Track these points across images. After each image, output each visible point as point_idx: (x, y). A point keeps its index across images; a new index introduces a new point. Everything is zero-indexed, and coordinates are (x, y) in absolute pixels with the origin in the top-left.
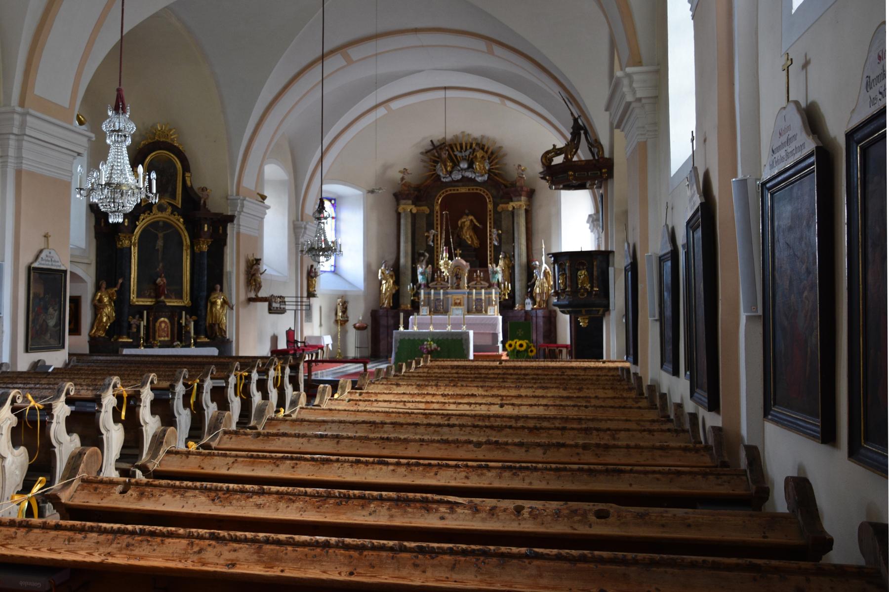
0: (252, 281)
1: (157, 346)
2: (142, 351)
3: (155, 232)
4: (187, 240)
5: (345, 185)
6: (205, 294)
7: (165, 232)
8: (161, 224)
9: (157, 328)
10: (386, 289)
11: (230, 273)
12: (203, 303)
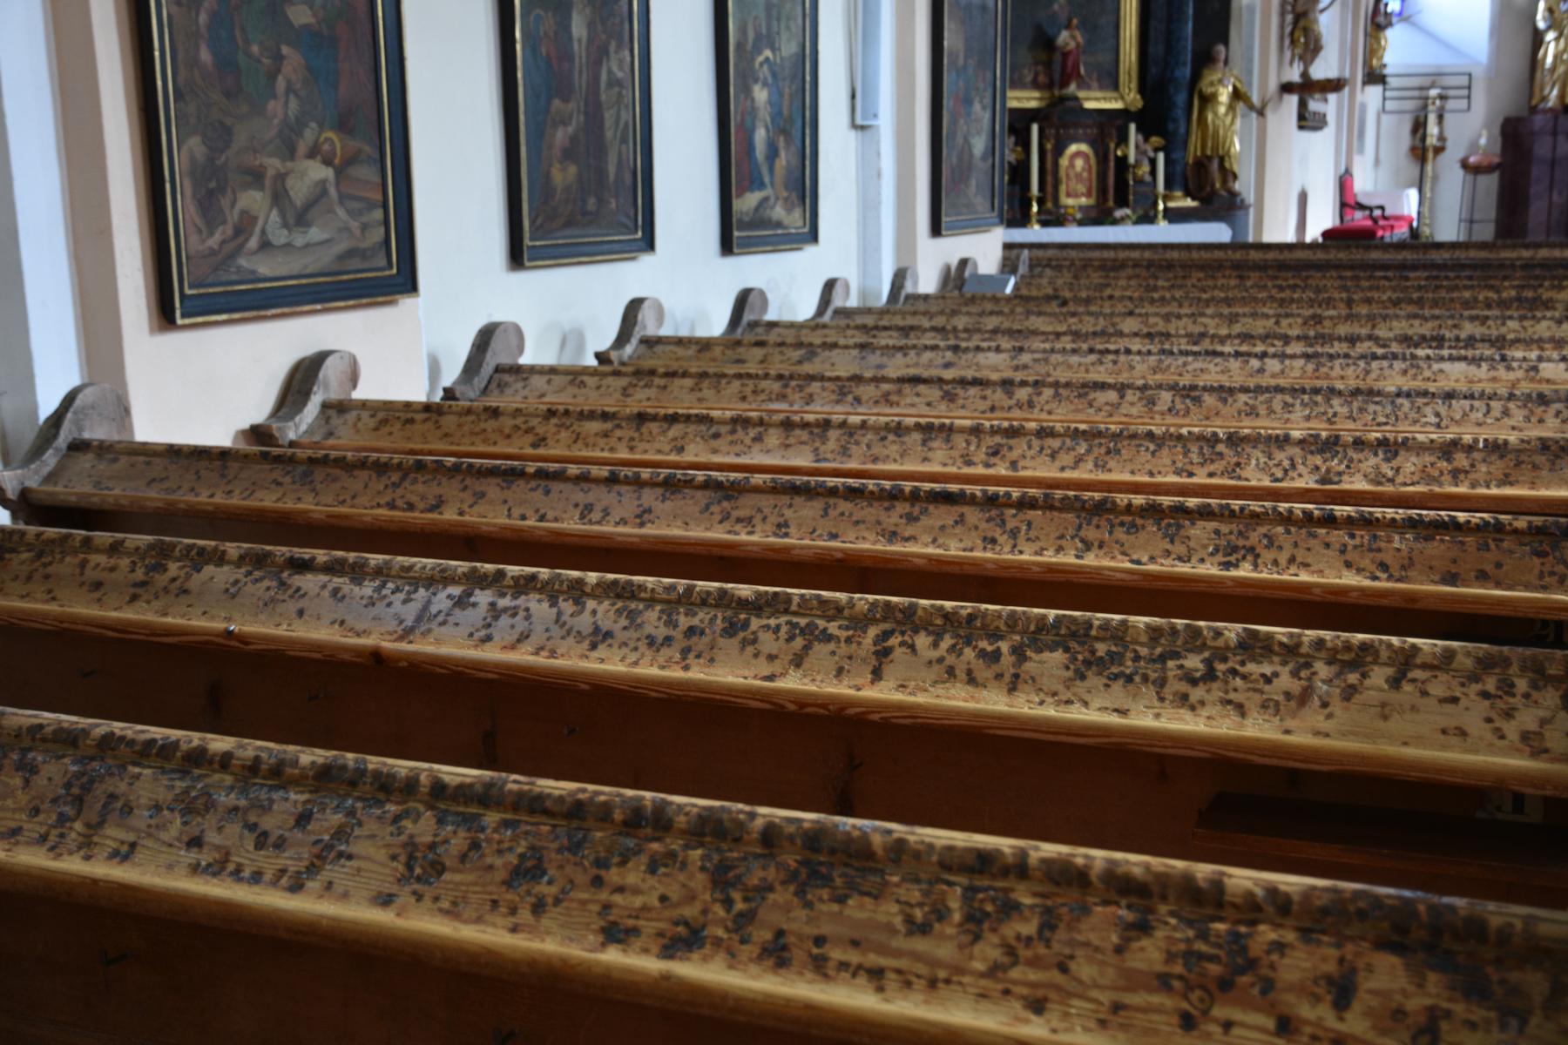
0: (1297, 34)
6: (1187, 71)
9: (1062, 173)
10: (1556, 57)
11: (1251, 9)
12: (1181, 98)
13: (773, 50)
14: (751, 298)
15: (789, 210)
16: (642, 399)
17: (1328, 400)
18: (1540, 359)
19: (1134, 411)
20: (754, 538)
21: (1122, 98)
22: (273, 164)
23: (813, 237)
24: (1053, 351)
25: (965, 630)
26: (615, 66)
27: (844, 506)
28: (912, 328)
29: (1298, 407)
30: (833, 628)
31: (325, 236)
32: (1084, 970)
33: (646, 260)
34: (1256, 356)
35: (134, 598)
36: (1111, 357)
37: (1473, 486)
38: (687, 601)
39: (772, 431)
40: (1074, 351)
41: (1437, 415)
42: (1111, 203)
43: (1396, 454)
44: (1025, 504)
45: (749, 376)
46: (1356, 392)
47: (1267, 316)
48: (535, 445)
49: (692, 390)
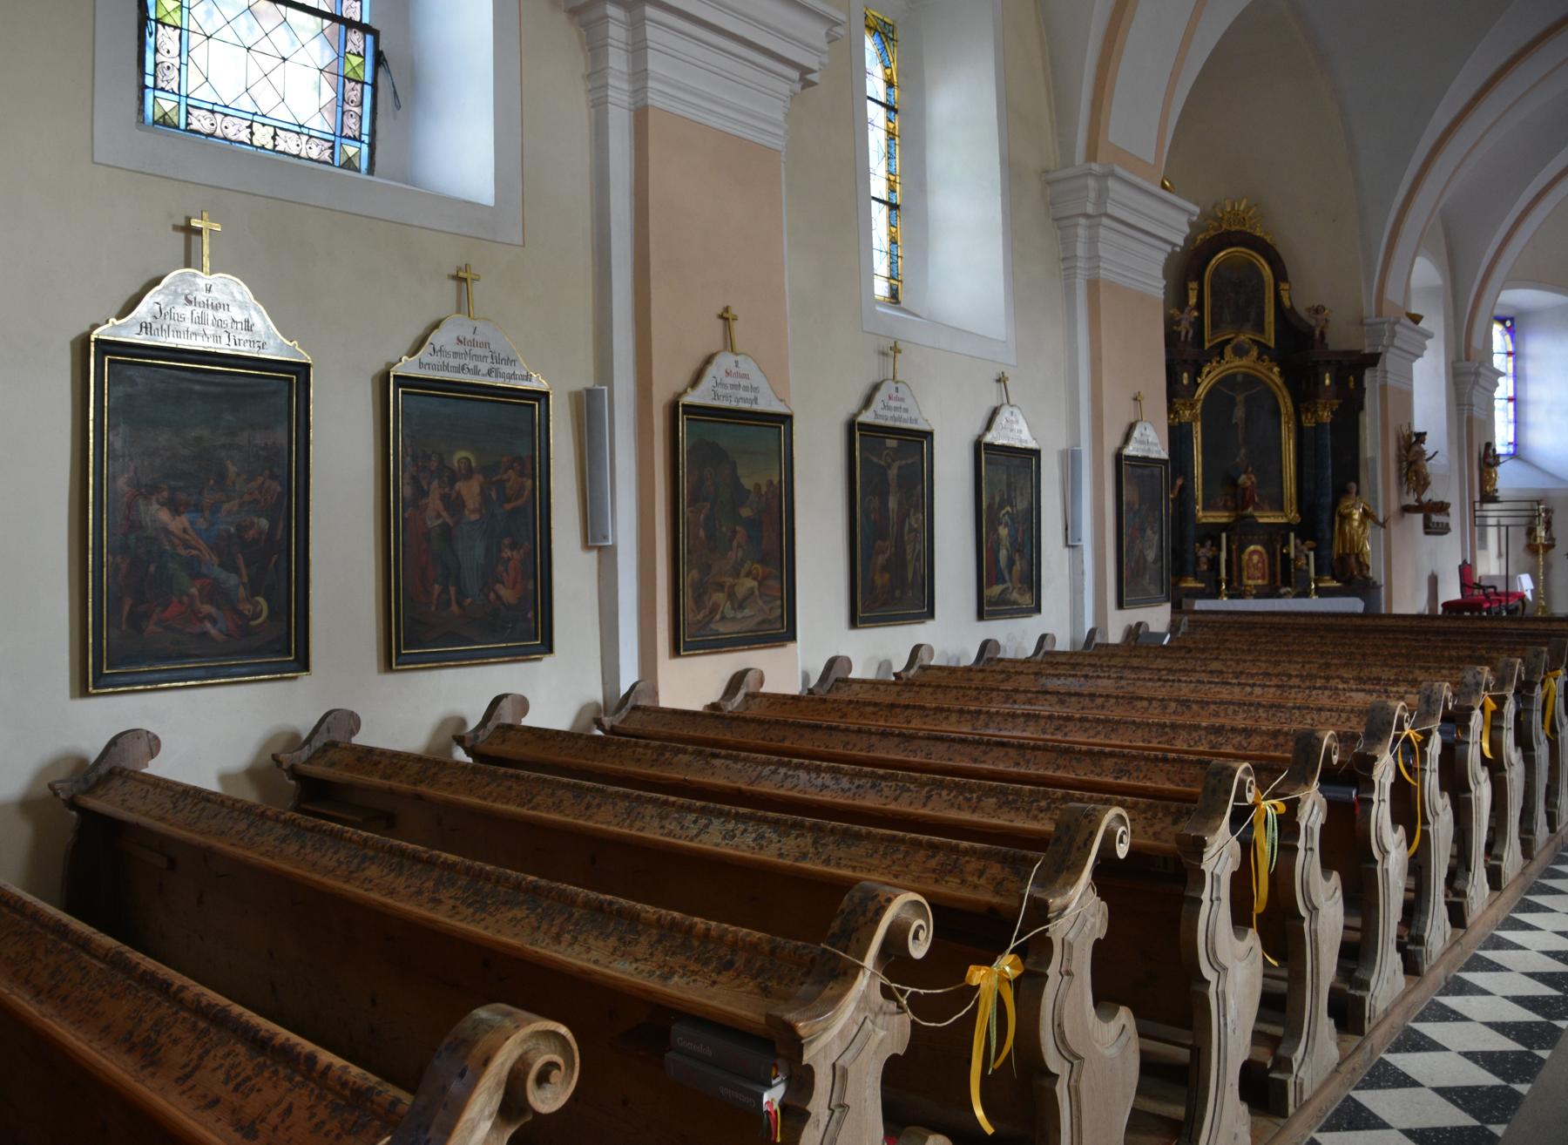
0: (1410, 474)
1: (1251, 594)
2: (1224, 604)
3: (1230, 393)
4: (1286, 405)
5: (1539, 288)
7: (1247, 393)
8: (1240, 378)
9: (1244, 564)
11: (1374, 460)
12: (1326, 516)
13: (1012, 507)
14: (837, 663)
15: (1022, 595)
16: (905, 698)
17: (1257, 709)
18: (1406, 692)
19: (1156, 712)
20: (917, 759)
21: (1286, 516)
22: (729, 581)
23: (1038, 609)
24: (1139, 679)
25: (961, 789)
26: (914, 520)
27: (957, 746)
28: (1078, 664)
29: (1241, 713)
30: (912, 787)
31: (752, 613)
32: (913, 867)
33: (930, 623)
34: (1250, 685)
35: (652, 766)
36: (1170, 684)
37: (1283, 752)
38: (859, 775)
39: (954, 714)
40: (1150, 680)
41: (1313, 719)
42: (1279, 583)
43: (1250, 736)
44: (1035, 748)
45: (961, 687)
46: (1272, 706)
47: (1298, 663)
48: (841, 717)
49: (932, 694)
